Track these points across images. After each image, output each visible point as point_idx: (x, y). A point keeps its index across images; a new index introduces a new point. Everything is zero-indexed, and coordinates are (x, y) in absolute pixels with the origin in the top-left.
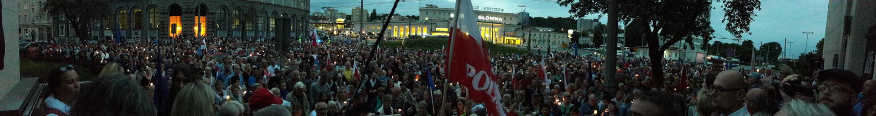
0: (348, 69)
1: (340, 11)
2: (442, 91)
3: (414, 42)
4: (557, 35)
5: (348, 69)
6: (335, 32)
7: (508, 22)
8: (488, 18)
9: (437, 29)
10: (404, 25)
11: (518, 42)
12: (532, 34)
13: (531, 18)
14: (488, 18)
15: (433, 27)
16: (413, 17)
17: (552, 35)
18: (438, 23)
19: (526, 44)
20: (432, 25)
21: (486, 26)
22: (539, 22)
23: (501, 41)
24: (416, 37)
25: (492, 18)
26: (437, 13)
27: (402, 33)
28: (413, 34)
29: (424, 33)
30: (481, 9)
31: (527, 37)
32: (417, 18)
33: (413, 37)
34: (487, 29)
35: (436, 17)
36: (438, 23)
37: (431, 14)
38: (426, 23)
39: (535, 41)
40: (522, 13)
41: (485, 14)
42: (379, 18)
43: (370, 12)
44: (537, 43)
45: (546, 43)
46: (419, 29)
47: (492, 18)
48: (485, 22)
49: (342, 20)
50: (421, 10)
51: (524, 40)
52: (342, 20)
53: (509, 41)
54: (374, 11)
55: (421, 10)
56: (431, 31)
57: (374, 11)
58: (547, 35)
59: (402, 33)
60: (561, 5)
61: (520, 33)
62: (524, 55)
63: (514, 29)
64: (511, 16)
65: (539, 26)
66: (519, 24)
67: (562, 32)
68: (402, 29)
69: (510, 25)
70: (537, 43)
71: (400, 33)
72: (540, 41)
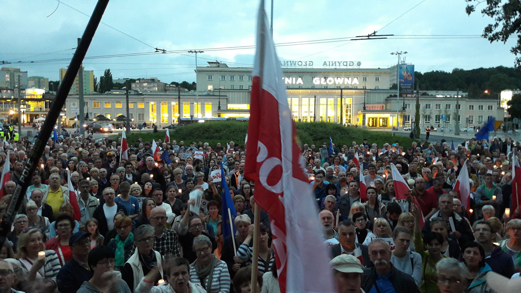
0: (55, 188)
1: (32, 72)
2: (251, 216)
3: (188, 132)
4: (476, 104)
5: (55, 188)
6: (24, 118)
7: (371, 85)
8: (331, 81)
9: (230, 106)
10: (169, 98)
11: (393, 121)
12: (422, 105)
13: (418, 75)
14: (331, 81)
15: (223, 102)
16: (185, 85)
17: (462, 103)
18: (230, 95)
19: (410, 125)
20: (219, 97)
21: (327, 96)
22: (436, 81)
23: (357, 121)
24: (192, 121)
25: (339, 81)
26: (228, 78)
27: (165, 116)
28: (186, 116)
29: (204, 113)
30: (318, 65)
31: (411, 111)
32: (192, 87)
33: (187, 122)
34: (331, 100)
35: (226, 84)
36: (230, 95)
37: (217, 78)
38: (209, 95)
39: (428, 118)
40: (399, 67)
41: (325, 73)
42: (119, 86)
43: (99, 75)
44: (433, 122)
45: (452, 122)
46: (197, 106)
47: (339, 81)
48: (326, 88)
49: (39, 92)
50: (199, 71)
51: (406, 118)
52: (39, 92)
53: (375, 120)
54: (108, 73)
55: (199, 71)
56: (219, 109)
57: (108, 73)
58: (453, 105)
59: (165, 116)
60: (492, 39)
61: (397, 104)
62: (411, 145)
63: (383, 97)
64: (378, 73)
65: (437, 88)
66: (394, 87)
67: (486, 97)
68: (164, 108)
69: (376, 91)
70: (433, 122)
71: (162, 115)
72: (438, 118)
